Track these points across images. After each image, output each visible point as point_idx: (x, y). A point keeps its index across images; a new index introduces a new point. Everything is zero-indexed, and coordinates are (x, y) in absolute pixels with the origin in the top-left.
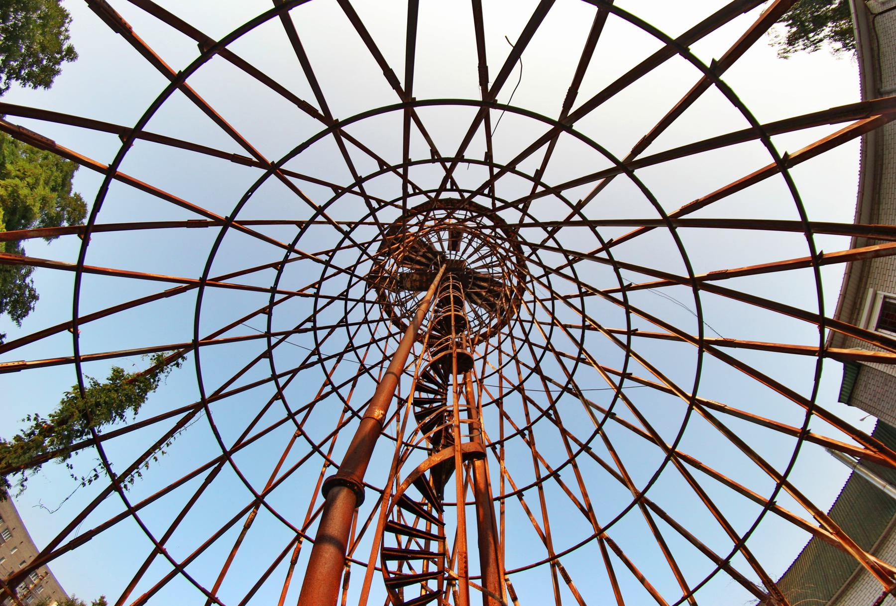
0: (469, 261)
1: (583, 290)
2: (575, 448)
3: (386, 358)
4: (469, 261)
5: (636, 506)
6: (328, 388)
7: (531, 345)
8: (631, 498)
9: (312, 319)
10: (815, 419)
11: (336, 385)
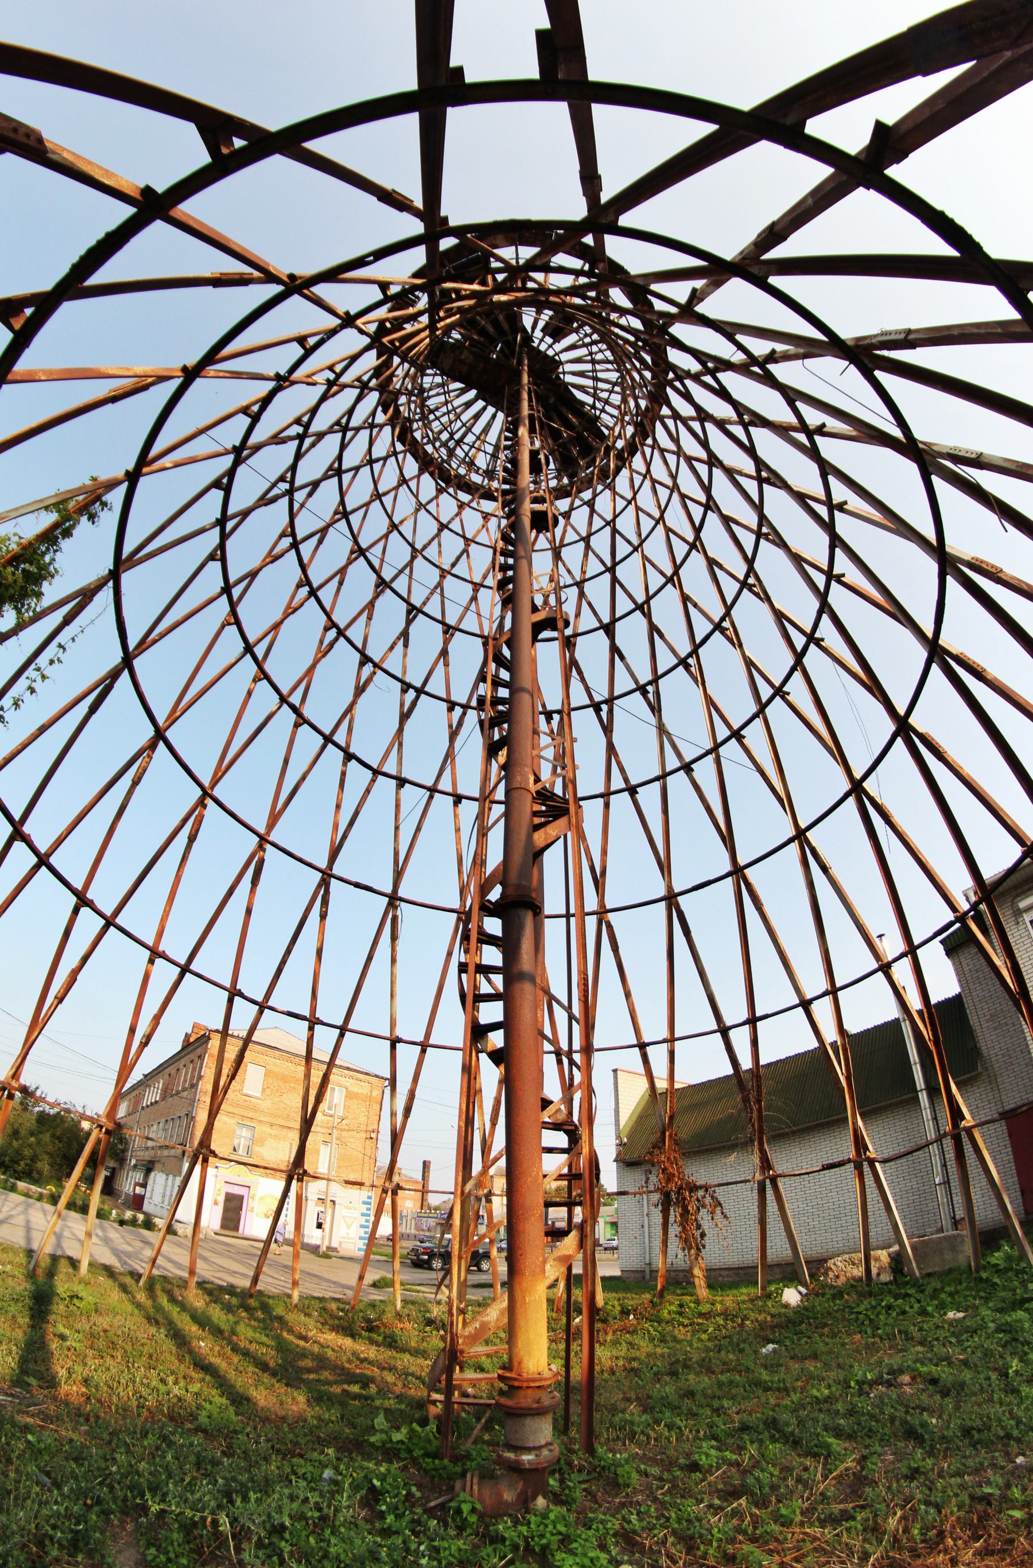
0: (568, 367)
1: (751, 580)
2: (617, 783)
4: (568, 367)
5: (663, 904)
7: (615, 532)
8: (662, 892)
10: (906, 963)
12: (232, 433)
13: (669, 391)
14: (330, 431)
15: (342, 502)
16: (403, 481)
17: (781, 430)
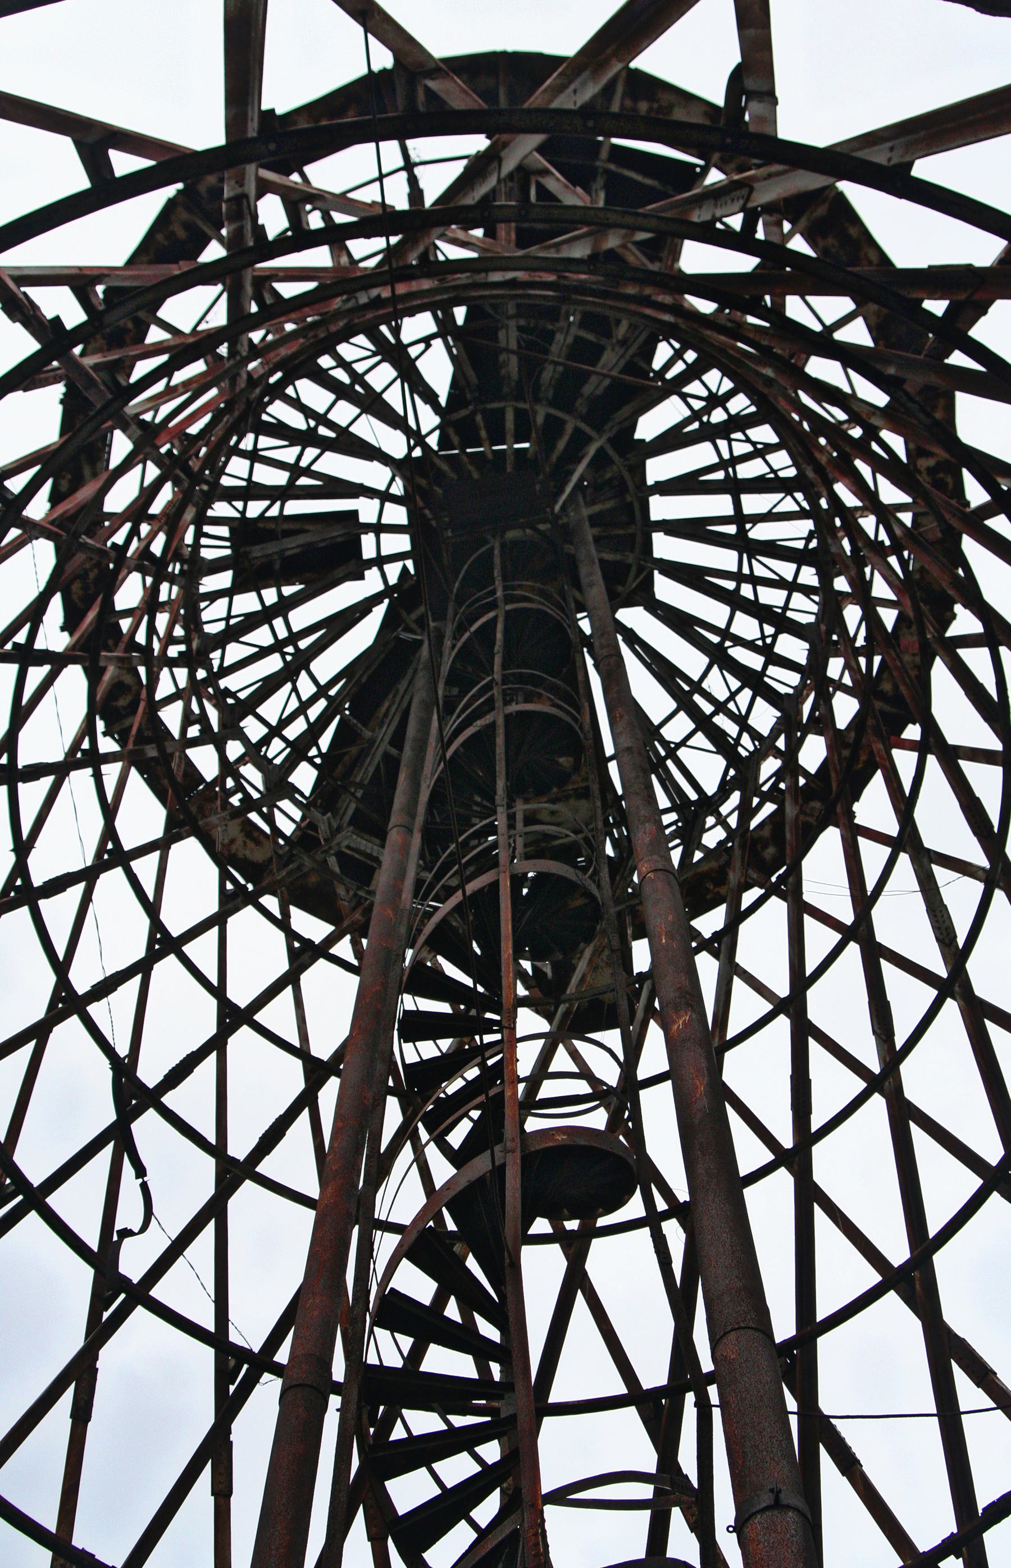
3: (316, 1072)
7: (804, 1032)
16: (112, 854)
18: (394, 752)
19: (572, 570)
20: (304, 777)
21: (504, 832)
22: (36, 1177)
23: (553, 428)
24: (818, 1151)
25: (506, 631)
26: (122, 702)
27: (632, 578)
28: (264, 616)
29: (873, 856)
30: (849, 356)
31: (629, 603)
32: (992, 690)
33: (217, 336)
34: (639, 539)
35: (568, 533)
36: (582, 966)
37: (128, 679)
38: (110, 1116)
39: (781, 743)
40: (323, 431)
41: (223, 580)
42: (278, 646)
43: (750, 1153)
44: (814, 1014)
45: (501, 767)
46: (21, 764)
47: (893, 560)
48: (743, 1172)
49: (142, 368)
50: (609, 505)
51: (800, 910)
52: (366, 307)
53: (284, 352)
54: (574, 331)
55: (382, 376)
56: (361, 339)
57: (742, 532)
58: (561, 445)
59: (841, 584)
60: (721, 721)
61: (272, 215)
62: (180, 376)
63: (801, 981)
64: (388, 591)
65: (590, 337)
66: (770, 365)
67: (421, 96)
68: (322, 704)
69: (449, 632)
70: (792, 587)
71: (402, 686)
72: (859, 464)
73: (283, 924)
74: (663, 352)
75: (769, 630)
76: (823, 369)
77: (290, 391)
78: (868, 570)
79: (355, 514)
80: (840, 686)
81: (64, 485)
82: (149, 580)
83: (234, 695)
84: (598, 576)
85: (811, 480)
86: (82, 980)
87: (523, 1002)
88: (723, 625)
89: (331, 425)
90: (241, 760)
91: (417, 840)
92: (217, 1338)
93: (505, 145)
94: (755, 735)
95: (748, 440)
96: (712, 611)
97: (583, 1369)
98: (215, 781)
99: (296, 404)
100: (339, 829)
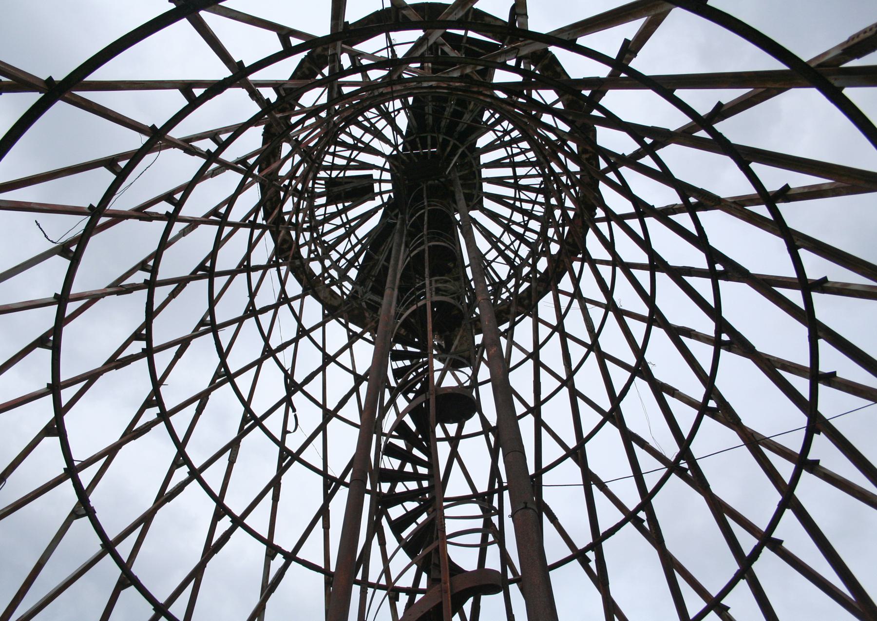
3: (359, 380)
6: (225, 523)
7: (538, 365)
9: (154, 399)
11: (238, 513)
12: (90, 188)
13: (603, 187)
14: (206, 220)
15: (211, 312)
17: (737, 207)
18: (386, 264)
19: (452, 195)
20: (353, 273)
21: (429, 283)
22: (259, 415)
23: (445, 143)
24: (543, 408)
25: (428, 217)
26: (285, 246)
27: (475, 200)
28: (339, 213)
29: (564, 300)
30: (555, 113)
31: (474, 209)
32: (608, 238)
33: (322, 108)
34: (477, 185)
35: (451, 182)
36: (456, 343)
37: (287, 238)
38: (284, 394)
39: (530, 261)
40: (359, 145)
41: (322, 200)
42: (343, 225)
43: (520, 409)
44: (542, 359)
45: (427, 264)
46: (252, 264)
47: (572, 191)
48: (518, 414)
49: (294, 120)
50: (466, 172)
51: (537, 321)
52: (377, 96)
53: (346, 114)
54: (453, 107)
55: (381, 124)
56: (373, 110)
57: (516, 182)
58: (449, 149)
59: (553, 201)
60: (508, 252)
61: (346, 61)
62: (308, 122)
63: (537, 346)
64: (384, 204)
65: (459, 109)
66: (527, 120)
67: (400, 16)
68: (360, 246)
69: (407, 218)
70: (534, 202)
71: (389, 239)
72: (559, 154)
73: (346, 326)
74: (487, 115)
75: (526, 218)
76: (547, 118)
77: (347, 130)
78: (563, 195)
79: (371, 175)
80: (552, 240)
81: (264, 166)
82: (296, 199)
83: (327, 243)
84: (462, 197)
85: (542, 162)
86: (274, 344)
87: (435, 356)
88: (508, 217)
89: (362, 143)
90: (330, 268)
91: (396, 291)
92: (324, 473)
93: (430, 34)
94: (521, 258)
95: (518, 147)
96: (505, 212)
97: (456, 487)
98: (320, 275)
99: (350, 135)
100: (366, 292)
